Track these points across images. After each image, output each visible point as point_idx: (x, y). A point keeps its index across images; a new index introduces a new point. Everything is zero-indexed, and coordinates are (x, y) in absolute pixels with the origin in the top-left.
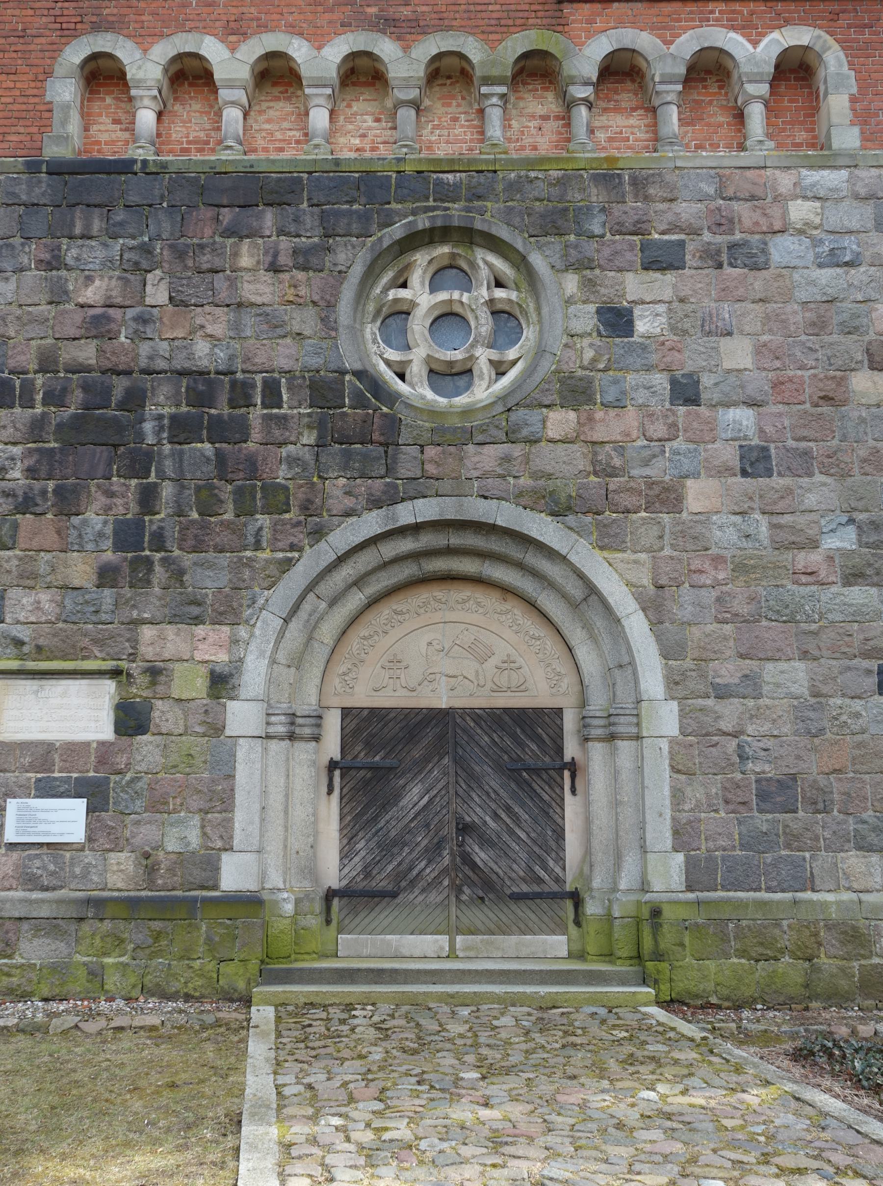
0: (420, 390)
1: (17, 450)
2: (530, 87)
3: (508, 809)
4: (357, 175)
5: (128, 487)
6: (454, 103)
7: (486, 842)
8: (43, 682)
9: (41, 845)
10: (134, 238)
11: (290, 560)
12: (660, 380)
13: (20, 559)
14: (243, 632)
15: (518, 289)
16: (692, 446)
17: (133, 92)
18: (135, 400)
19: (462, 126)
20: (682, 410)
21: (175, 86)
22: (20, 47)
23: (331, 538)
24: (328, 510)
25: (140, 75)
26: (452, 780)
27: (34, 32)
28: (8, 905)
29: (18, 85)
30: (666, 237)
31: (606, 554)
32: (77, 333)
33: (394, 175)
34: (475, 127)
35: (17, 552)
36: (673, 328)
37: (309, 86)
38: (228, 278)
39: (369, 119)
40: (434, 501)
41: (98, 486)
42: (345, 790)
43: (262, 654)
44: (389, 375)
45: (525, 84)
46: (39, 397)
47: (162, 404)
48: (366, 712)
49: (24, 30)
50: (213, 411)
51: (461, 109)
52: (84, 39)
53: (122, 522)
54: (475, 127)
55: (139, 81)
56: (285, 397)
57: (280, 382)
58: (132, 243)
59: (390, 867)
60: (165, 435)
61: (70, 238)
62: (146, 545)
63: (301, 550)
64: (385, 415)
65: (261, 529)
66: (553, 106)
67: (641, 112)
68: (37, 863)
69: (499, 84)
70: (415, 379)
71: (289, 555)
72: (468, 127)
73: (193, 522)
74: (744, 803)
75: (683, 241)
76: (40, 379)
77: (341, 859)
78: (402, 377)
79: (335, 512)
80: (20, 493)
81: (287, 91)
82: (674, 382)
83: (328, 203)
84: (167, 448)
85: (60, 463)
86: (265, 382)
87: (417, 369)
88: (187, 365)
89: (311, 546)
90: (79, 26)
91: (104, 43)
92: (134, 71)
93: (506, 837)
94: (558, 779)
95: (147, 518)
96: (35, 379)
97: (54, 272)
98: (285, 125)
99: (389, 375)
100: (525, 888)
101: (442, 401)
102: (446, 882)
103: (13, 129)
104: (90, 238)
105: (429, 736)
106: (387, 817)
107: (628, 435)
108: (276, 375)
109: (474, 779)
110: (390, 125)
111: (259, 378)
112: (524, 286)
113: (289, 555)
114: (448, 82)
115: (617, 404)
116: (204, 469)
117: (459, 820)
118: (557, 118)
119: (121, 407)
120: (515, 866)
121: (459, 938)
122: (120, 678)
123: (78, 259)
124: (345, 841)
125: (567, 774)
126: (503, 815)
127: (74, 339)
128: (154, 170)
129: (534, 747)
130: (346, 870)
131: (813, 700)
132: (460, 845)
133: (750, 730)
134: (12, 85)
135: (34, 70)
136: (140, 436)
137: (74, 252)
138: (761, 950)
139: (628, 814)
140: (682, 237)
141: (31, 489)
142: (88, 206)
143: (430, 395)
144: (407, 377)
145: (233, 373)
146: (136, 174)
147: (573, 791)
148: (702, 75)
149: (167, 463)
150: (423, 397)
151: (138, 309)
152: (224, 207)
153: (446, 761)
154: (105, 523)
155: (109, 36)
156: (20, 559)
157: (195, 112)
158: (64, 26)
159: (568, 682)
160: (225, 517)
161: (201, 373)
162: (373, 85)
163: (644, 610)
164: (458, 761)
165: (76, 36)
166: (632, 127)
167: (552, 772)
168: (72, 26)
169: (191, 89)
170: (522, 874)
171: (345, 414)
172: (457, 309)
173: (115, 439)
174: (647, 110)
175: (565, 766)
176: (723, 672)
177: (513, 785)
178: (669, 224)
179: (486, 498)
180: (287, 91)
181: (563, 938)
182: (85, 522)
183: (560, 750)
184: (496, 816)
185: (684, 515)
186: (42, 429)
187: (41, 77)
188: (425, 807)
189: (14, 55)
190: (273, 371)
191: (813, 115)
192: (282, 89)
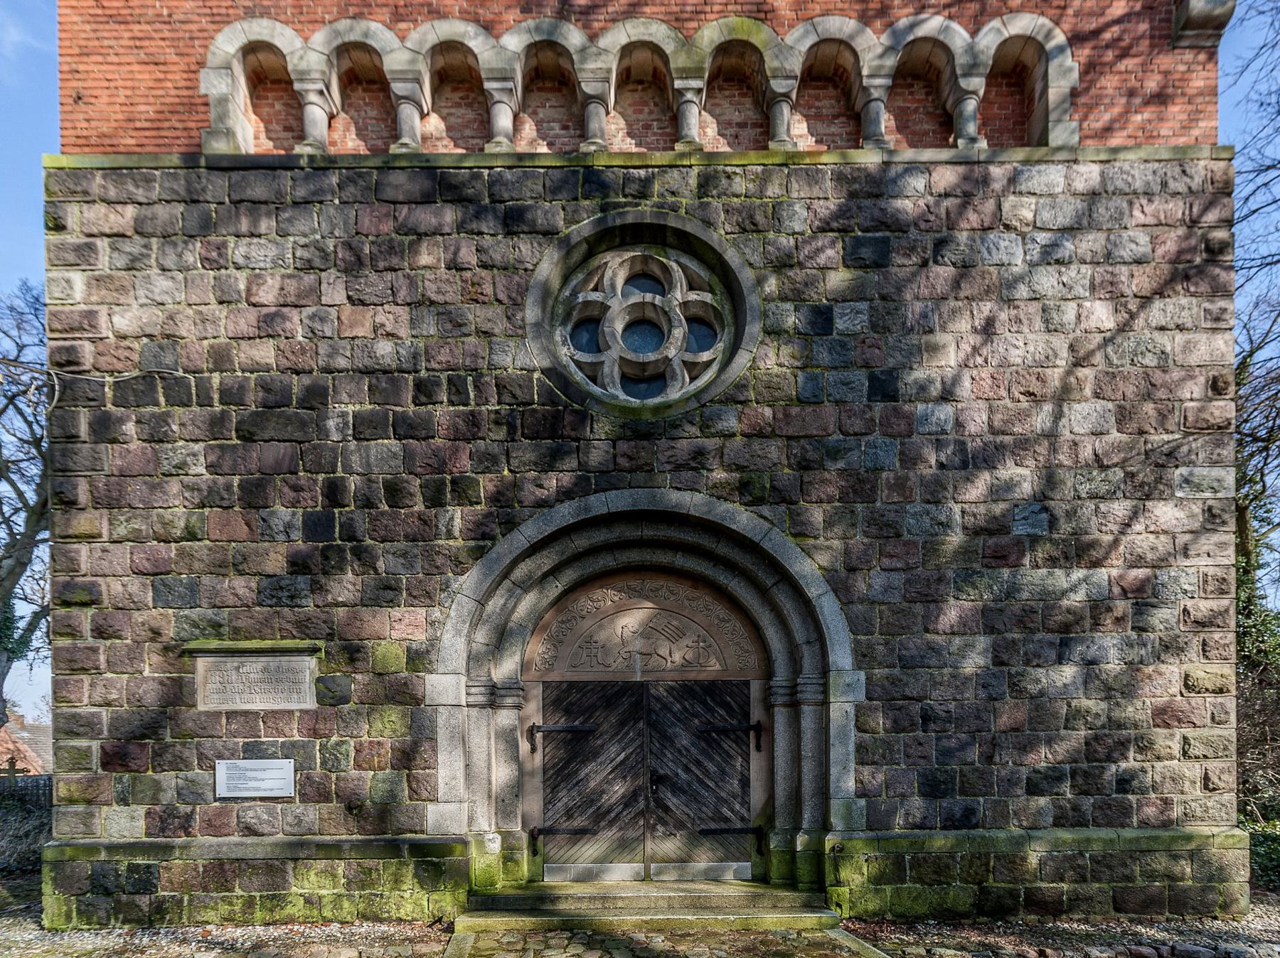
0: (612, 391)
1: (198, 447)
2: (727, 93)
3: (698, 763)
4: (542, 170)
5: (315, 481)
6: (646, 110)
7: (677, 789)
8: (243, 659)
9: (254, 799)
10: (305, 236)
11: (483, 547)
12: (860, 378)
13: (210, 549)
14: (436, 613)
15: (712, 291)
16: (887, 440)
17: (297, 86)
18: (316, 398)
19: (655, 134)
20: (879, 407)
21: (348, 91)
22: (167, 34)
23: (523, 528)
24: (520, 502)
25: (303, 66)
26: (646, 740)
27: (182, 17)
28: (224, 849)
29: (170, 76)
30: (869, 235)
31: (799, 540)
32: (253, 332)
33: (582, 170)
34: (668, 135)
35: (207, 542)
36: (874, 327)
37: (489, 79)
38: (408, 277)
39: (556, 126)
40: (626, 492)
41: (284, 480)
42: (547, 750)
43: (458, 633)
44: (579, 376)
45: (721, 89)
46: (216, 396)
47: (348, 405)
48: (565, 685)
49: (170, 15)
50: (398, 409)
51: (653, 117)
52: (237, 25)
53: (312, 514)
54: (668, 135)
55: (303, 72)
56: (472, 395)
57: (466, 380)
58: (303, 241)
59: (591, 810)
60: (350, 432)
61: (238, 236)
62: (337, 535)
63: (493, 538)
64: (576, 412)
65: (452, 519)
66: (750, 113)
67: (843, 119)
68: (251, 814)
69: (695, 78)
70: (607, 380)
71: (481, 543)
72: (661, 135)
73: (383, 513)
74: (924, 757)
75: (888, 238)
76: (216, 379)
77: (545, 805)
78: (594, 380)
79: (526, 503)
80: (204, 487)
81: (468, 97)
82: (872, 378)
83: (512, 199)
84: (353, 444)
85: (244, 459)
86: (450, 380)
87: (611, 370)
88: (368, 362)
89: (503, 536)
90: (231, 11)
91: (261, 29)
92: (295, 61)
93: (696, 786)
94: (745, 739)
95: (336, 511)
96: (210, 378)
97: (223, 271)
98: (468, 132)
99: (579, 376)
100: (713, 826)
101: (635, 402)
102: (641, 822)
103: (166, 124)
104: (259, 236)
105: (626, 703)
106: (587, 771)
107: (825, 430)
108: (462, 373)
109: (667, 739)
110: (578, 132)
111: (443, 377)
112: (719, 288)
113: (481, 543)
114: (640, 87)
115: (813, 400)
116: (392, 464)
117: (654, 773)
118: (755, 125)
119: (301, 405)
120: (704, 808)
121: (653, 866)
122: (318, 654)
123: (247, 258)
124: (548, 791)
125: (752, 734)
126: (694, 768)
127: (250, 338)
128: (322, 165)
129: (722, 712)
130: (550, 814)
131: (996, 669)
132: (654, 792)
133: (934, 694)
134: (162, 76)
135: (186, 59)
136: (323, 432)
137: (242, 250)
138: (934, 877)
139: (808, 768)
140: (888, 234)
141: (215, 483)
142: (254, 202)
143: (622, 396)
144: (599, 380)
145: (417, 371)
146: (302, 169)
147: (758, 748)
148: (909, 81)
149: (353, 458)
150: (616, 397)
151: (313, 309)
152: (401, 203)
153: (641, 725)
154: (294, 514)
155: (265, 22)
156: (210, 549)
157: (371, 118)
158: (215, 11)
159: (753, 660)
160: (416, 508)
161: (385, 372)
162: (560, 90)
163: (835, 591)
164: (651, 724)
165: (229, 23)
166: (833, 135)
167: (739, 733)
168: (223, 11)
169: (366, 95)
170: (710, 814)
171: (534, 410)
172: (650, 314)
173: (298, 435)
174: (849, 117)
175: (752, 728)
176: (911, 645)
177: (703, 744)
178: (873, 220)
179: (679, 489)
180: (468, 97)
181: (749, 864)
182: (273, 513)
183: (747, 715)
184: (687, 769)
185: (878, 504)
186: (223, 426)
187: (193, 68)
188: (622, 762)
189: (162, 43)
190: (459, 369)
191: (1023, 123)
192: (461, 94)
